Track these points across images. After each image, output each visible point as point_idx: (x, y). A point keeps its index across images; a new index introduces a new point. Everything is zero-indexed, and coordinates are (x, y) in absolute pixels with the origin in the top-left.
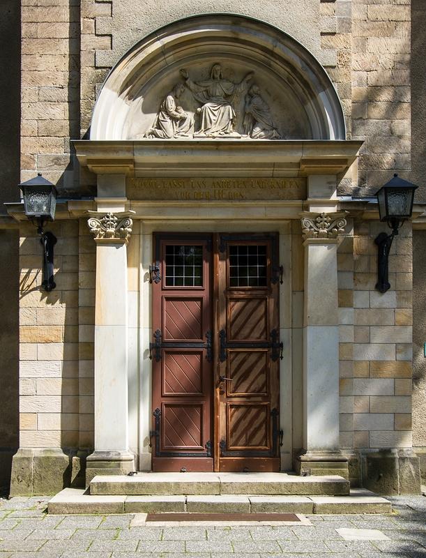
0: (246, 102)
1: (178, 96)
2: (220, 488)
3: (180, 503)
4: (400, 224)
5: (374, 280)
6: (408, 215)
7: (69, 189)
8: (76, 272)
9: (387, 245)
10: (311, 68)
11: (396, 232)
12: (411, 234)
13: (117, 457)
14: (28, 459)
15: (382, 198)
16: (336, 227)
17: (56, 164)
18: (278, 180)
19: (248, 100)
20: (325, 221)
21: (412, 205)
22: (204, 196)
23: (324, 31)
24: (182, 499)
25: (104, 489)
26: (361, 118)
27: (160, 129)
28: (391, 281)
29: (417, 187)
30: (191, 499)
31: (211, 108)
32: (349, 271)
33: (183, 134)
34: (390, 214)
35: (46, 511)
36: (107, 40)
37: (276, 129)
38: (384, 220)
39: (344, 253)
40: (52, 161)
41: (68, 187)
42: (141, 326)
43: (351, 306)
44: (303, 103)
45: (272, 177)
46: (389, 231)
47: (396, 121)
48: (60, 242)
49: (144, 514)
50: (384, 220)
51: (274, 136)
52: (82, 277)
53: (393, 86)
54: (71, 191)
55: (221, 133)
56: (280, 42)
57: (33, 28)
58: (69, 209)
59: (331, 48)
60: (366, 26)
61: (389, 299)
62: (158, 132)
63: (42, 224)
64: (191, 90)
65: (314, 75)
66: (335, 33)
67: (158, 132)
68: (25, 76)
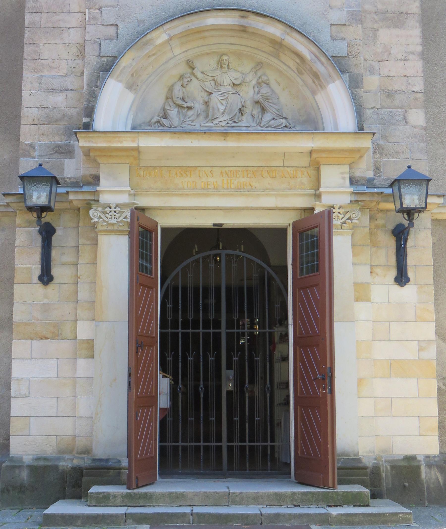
0: (255, 92)
1: (185, 85)
2: (232, 500)
3: (184, 515)
4: (416, 215)
5: (393, 273)
6: (423, 208)
7: (70, 178)
8: (76, 264)
9: (404, 237)
10: (320, 60)
11: (412, 224)
12: (429, 225)
13: (117, 465)
14: (19, 467)
15: (396, 189)
16: (349, 218)
17: (56, 152)
18: (288, 169)
19: (257, 89)
20: (339, 213)
21: (427, 195)
22: (212, 187)
23: (333, 23)
24: (187, 510)
25: (103, 500)
26: (374, 107)
27: (166, 118)
28: (410, 274)
29: (431, 180)
30: (196, 510)
31: (219, 98)
32: (366, 264)
33: (190, 123)
34: (404, 206)
35: (43, 134)
36: (112, 30)
37: (286, 118)
38: (399, 211)
39: (360, 245)
40: (53, 149)
41: (69, 175)
42: (28, 456)
43: (368, 300)
44: (314, 93)
45: (283, 167)
46: (406, 223)
47: (411, 110)
48: (59, 232)
49: (146, 526)
50: (399, 211)
51: (284, 125)
52: (83, 270)
53: (405, 76)
54: (72, 180)
55: (230, 122)
56: (288, 34)
57: (37, 17)
58: (69, 199)
59: (342, 39)
60: (376, 17)
61: (408, 292)
62: (164, 121)
63: (41, 215)
64: (198, 80)
65: (323, 67)
66: (345, 25)
67: (164, 121)
68: (27, 64)
